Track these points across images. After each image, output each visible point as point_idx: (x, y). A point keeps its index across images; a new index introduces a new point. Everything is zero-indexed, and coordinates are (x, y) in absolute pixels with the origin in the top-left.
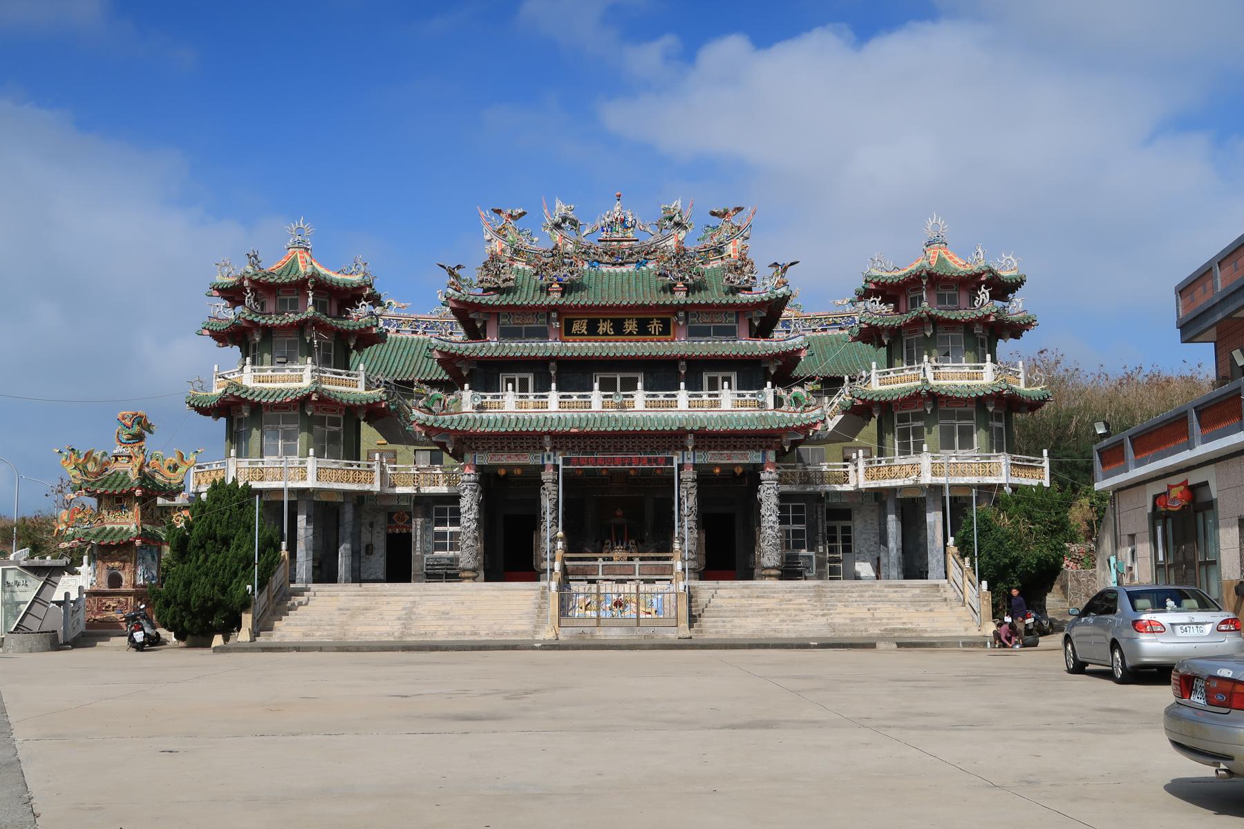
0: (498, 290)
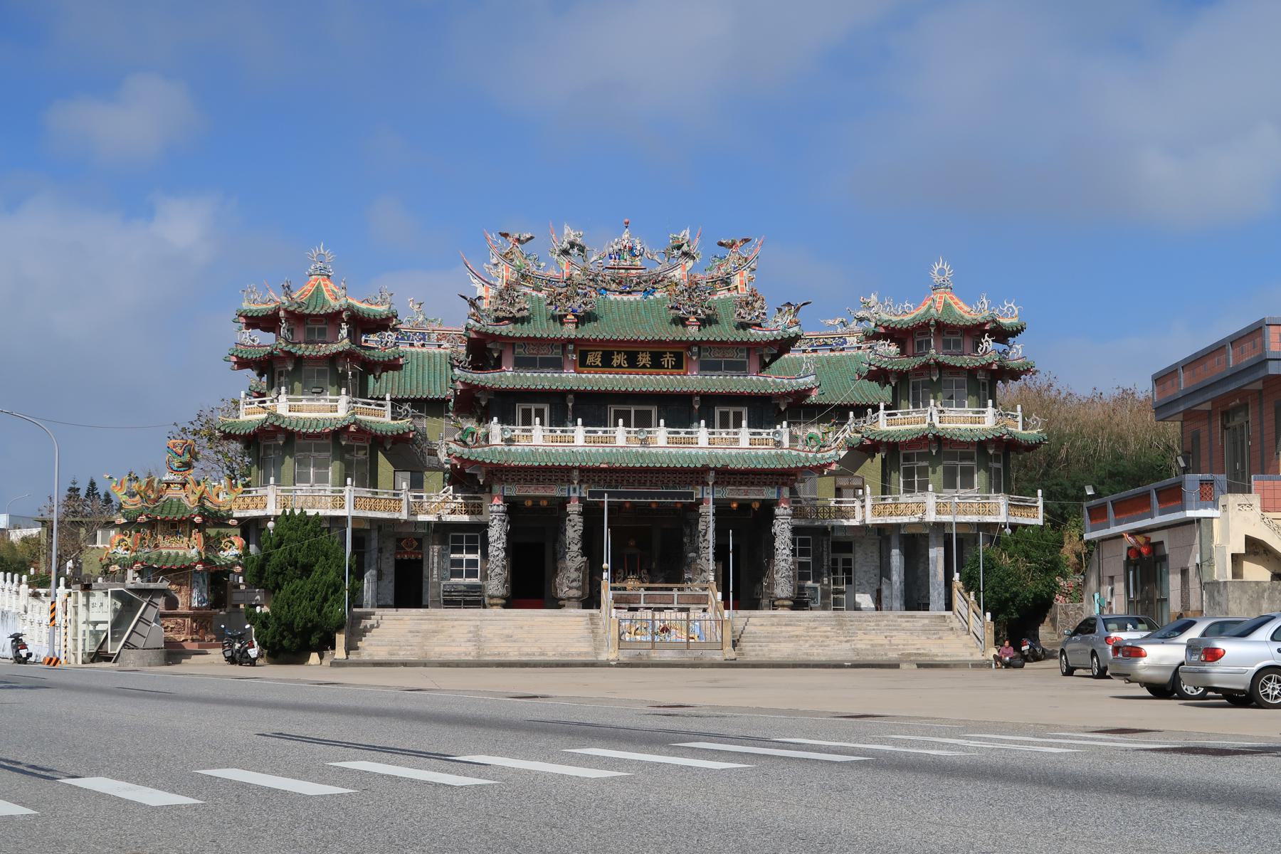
0: (514, 320)
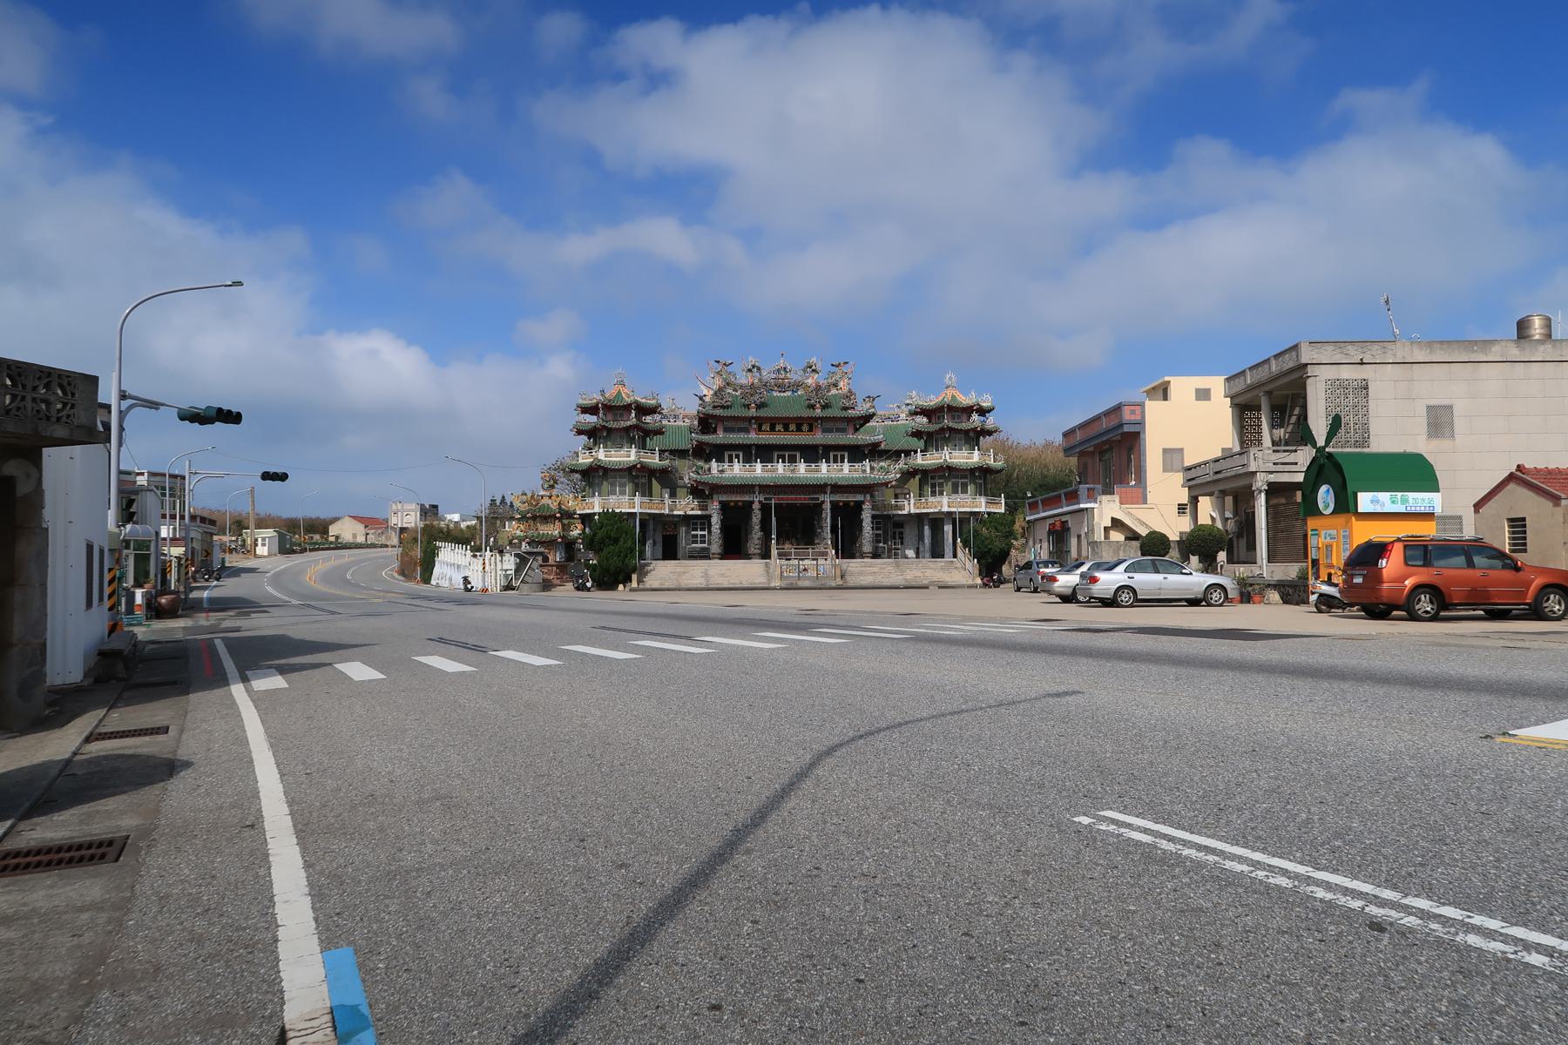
0: (723, 407)
